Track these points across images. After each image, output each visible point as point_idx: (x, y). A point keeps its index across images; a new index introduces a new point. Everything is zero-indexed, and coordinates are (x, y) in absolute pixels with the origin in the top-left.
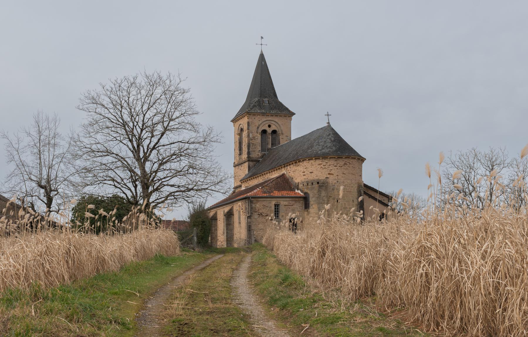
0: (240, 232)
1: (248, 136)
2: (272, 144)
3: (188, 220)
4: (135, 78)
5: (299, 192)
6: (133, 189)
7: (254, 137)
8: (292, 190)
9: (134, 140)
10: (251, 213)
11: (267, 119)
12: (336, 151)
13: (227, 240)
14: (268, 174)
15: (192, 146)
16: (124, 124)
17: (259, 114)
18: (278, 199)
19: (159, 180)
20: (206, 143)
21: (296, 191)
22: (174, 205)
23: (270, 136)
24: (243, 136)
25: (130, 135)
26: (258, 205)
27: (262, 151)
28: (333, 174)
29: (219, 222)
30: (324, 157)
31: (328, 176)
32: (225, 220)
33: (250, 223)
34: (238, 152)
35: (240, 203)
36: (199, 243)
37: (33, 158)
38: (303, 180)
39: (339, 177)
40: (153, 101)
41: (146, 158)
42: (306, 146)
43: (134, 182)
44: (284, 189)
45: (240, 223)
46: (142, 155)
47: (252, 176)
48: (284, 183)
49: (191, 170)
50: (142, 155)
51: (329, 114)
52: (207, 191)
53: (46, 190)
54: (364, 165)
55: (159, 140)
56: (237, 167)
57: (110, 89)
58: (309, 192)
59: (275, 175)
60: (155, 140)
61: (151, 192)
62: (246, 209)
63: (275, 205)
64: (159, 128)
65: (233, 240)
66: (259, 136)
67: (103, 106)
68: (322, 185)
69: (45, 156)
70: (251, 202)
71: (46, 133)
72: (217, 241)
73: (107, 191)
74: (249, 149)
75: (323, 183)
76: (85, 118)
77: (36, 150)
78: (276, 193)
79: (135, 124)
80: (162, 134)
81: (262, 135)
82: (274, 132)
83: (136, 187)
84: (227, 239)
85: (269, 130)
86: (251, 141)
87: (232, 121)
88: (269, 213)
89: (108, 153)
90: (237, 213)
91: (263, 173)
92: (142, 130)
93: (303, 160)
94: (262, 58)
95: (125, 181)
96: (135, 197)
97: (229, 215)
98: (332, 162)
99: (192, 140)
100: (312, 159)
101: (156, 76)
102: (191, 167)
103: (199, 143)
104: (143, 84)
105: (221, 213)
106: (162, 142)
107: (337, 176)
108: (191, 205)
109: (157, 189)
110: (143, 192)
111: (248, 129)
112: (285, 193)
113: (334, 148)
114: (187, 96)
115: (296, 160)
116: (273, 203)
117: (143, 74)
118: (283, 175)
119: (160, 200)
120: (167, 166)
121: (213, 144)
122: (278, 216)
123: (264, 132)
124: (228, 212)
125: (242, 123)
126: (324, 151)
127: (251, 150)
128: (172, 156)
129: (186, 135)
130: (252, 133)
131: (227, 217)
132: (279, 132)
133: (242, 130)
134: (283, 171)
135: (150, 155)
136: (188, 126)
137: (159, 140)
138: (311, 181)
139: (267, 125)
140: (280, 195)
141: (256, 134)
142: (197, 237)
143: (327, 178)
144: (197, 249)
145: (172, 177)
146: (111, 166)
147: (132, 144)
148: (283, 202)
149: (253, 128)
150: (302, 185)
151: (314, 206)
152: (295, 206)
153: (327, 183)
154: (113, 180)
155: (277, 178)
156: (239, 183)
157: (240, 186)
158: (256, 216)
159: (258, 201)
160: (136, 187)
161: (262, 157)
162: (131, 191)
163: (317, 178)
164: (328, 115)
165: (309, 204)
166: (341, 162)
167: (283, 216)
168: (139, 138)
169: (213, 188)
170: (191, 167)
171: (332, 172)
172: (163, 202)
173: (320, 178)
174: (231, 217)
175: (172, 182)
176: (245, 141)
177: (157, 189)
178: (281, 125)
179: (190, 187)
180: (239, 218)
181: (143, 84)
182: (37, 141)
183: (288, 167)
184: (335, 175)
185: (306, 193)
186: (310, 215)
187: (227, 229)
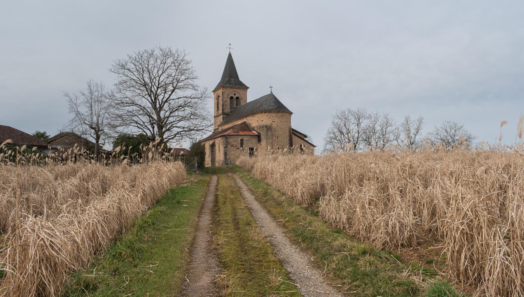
0: (220, 156)
1: (223, 100)
3: (188, 149)
4: (153, 52)
6: (151, 129)
9: (152, 96)
12: (277, 108)
15: (193, 100)
16: (145, 85)
17: (229, 87)
19: (170, 123)
20: (202, 99)
22: (180, 140)
25: (150, 93)
26: (231, 140)
30: (270, 111)
35: (219, 139)
36: (198, 167)
37: (87, 110)
40: (166, 67)
41: (161, 108)
42: (258, 105)
43: (152, 124)
46: (158, 106)
47: (225, 122)
48: (246, 127)
49: (192, 117)
50: (158, 106)
52: (203, 131)
53: (95, 130)
54: (292, 116)
55: (170, 95)
57: (134, 58)
59: (239, 122)
60: (167, 96)
61: (164, 132)
64: (171, 88)
66: (229, 100)
67: (129, 70)
68: (268, 128)
69: (96, 108)
70: (227, 138)
71: (96, 94)
73: (133, 131)
76: (116, 78)
77: (88, 105)
78: (241, 133)
79: (153, 84)
80: (173, 91)
82: (237, 98)
83: (153, 128)
85: (235, 97)
89: (133, 103)
92: (158, 88)
94: (230, 55)
95: (146, 124)
96: (153, 135)
97: (213, 146)
98: (274, 114)
99: (193, 96)
101: (167, 50)
102: (192, 114)
103: (198, 98)
104: (159, 55)
105: (207, 145)
106: (171, 97)
108: (191, 140)
109: (168, 130)
110: (159, 132)
112: (246, 133)
113: (275, 107)
114: (189, 66)
115: (253, 113)
116: (240, 139)
117: (158, 47)
118: (245, 122)
119: (171, 137)
120: (176, 113)
121: (208, 99)
123: (232, 98)
128: (179, 107)
129: (189, 92)
132: (240, 98)
133: (219, 96)
134: (245, 120)
135: (163, 106)
136: (190, 86)
137: (170, 95)
142: (197, 163)
144: (197, 172)
145: (180, 121)
146: (136, 114)
147: (151, 98)
148: (245, 138)
149: (226, 95)
154: (137, 123)
155: (242, 124)
156: (217, 127)
157: (218, 129)
158: (229, 146)
160: (153, 128)
161: (231, 112)
162: (150, 131)
166: (280, 115)
168: (156, 94)
169: (207, 129)
170: (192, 114)
172: (172, 138)
175: (178, 125)
176: (221, 103)
177: (168, 130)
179: (192, 128)
180: (219, 148)
181: (159, 55)
182: (89, 98)
185: (259, 133)
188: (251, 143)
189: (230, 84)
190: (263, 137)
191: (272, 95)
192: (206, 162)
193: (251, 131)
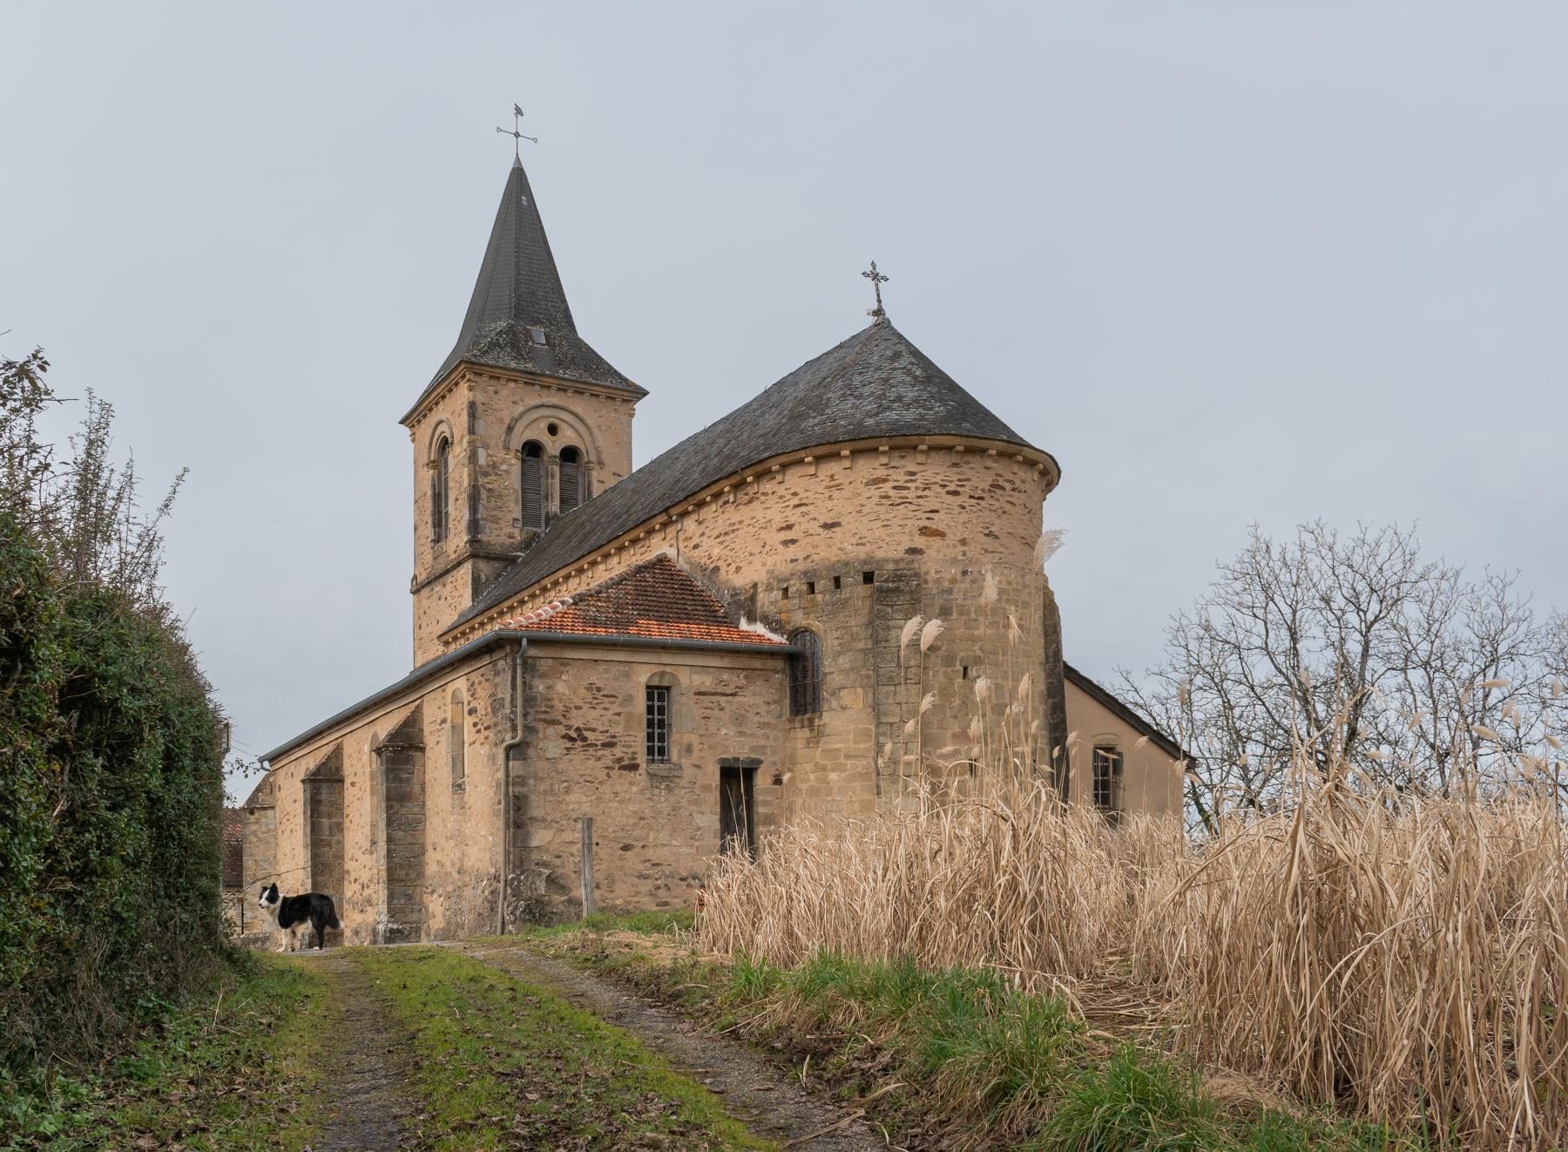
1: (473, 458)
2: (562, 501)
5: (760, 628)
7: (494, 466)
8: (728, 621)
10: (529, 729)
11: (545, 400)
13: (391, 879)
17: (513, 376)
21: (744, 625)
23: (557, 469)
24: (451, 461)
26: (565, 686)
27: (524, 524)
28: (942, 535)
29: (350, 793)
31: (920, 542)
32: (380, 778)
33: (521, 781)
34: (429, 532)
35: (459, 683)
38: (784, 569)
39: (972, 550)
44: (688, 618)
45: (458, 787)
48: (672, 594)
51: (881, 271)
54: (1056, 509)
56: (425, 592)
58: (816, 625)
62: (496, 705)
63: (650, 690)
65: (421, 875)
66: (513, 465)
68: (889, 588)
70: (529, 667)
72: (341, 881)
74: (474, 509)
75: (898, 577)
78: (655, 631)
81: (523, 461)
82: (570, 454)
84: (389, 870)
85: (553, 446)
86: (482, 480)
87: (402, 422)
88: (618, 730)
90: (445, 737)
91: (547, 582)
93: (785, 467)
94: (518, 181)
97: (402, 751)
98: (936, 470)
100: (836, 456)
107: (963, 542)
111: (472, 431)
112: (695, 632)
116: (643, 676)
122: (662, 751)
123: (532, 450)
124: (393, 737)
125: (443, 416)
126: (891, 415)
127: (481, 513)
130: (486, 447)
131: (389, 761)
134: (660, 546)
138: (832, 567)
139: (544, 425)
140: (678, 639)
141: (501, 454)
143: (913, 551)
149: (491, 430)
150: (777, 594)
151: (846, 697)
152: (746, 699)
153: (917, 575)
155: (622, 579)
158: (551, 744)
159: (564, 662)
161: (526, 545)
163: (861, 553)
164: (875, 277)
165: (816, 689)
167: (689, 749)
171: (938, 522)
173: (880, 554)
174: (409, 760)
176: (459, 477)
178: (596, 431)
180: (457, 762)
183: (690, 524)
184: (952, 538)
185: (794, 634)
186: (827, 743)
187: (389, 824)
188: (739, 719)
189: (519, 356)
190: (836, 669)
191: (882, 340)
192: (350, 890)
193: (728, 621)
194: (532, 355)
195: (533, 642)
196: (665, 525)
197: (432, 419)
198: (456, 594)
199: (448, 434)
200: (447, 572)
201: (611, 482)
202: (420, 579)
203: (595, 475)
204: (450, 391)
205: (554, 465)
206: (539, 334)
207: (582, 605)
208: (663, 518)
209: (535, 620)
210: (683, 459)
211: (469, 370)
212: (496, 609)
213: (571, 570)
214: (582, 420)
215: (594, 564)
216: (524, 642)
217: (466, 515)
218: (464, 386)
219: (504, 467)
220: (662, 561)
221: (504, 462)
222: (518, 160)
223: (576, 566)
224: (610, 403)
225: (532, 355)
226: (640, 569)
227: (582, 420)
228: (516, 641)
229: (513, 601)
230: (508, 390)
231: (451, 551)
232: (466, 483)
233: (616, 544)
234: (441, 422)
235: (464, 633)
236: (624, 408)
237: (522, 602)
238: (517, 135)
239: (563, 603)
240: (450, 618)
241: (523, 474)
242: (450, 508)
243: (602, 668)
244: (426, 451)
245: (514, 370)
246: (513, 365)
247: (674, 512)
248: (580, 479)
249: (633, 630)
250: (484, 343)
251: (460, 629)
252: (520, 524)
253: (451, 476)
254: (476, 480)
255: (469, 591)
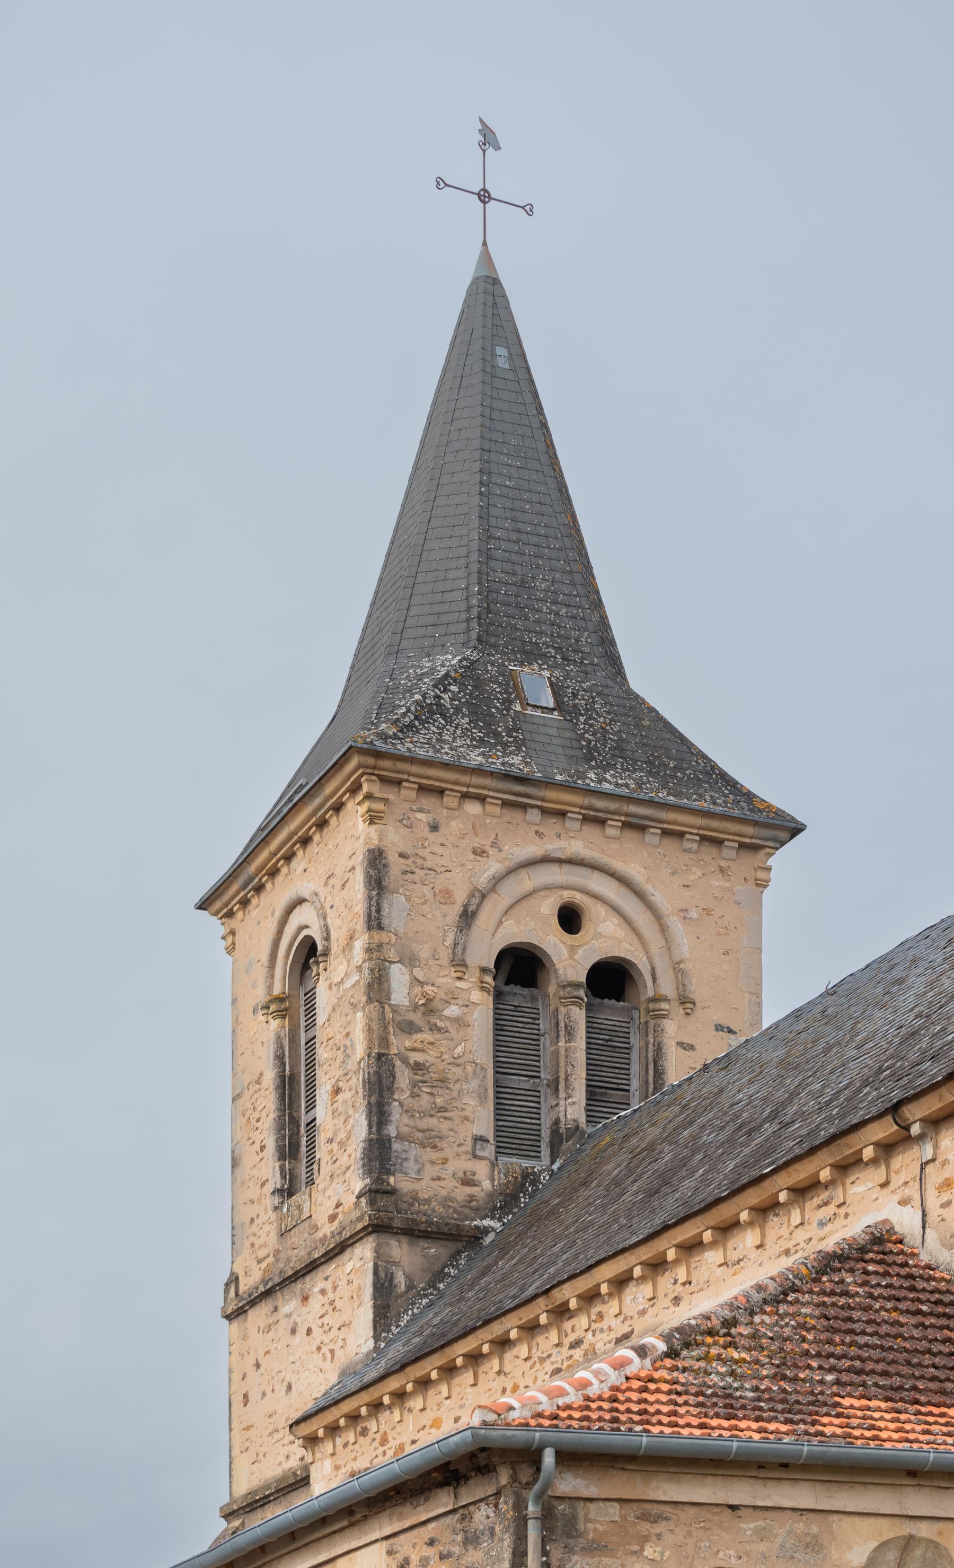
1: (377, 987)
2: (592, 1094)
11: (554, 846)
14: (636, 1295)
17: (471, 786)
18: (919, 1501)
23: (579, 1015)
24: (324, 998)
27: (500, 1150)
34: (268, 1169)
56: (258, 1316)
66: (474, 1006)
74: (378, 1113)
81: (498, 996)
85: (571, 960)
87: (203, 905)
91: (569, 1294)
94: (488, 309)
111: (374, 921)
123: (520, 967)
125: (303, 888)
127: (398, 1122)
130: (410, 960)
134: (869, 1204)
139: (549, 907)
141: (446, 979)
149: (422, 918)
155: (784, 1293)
159: (651, 1512)
161: (506, 1201)
178: (675, 924)
189: (490, 737)
194: (518, 734)
195: (570, 1458)
196: (887, 1149)
197: (277, 896)
198: (332, 1320)
199: (316, 933)
200: (312, 1267)
201: (713, 1047)
202: (245, 1285)
203: (672, 1029)
204: (322, 824)
205: (569, 1005)
206: (537, 685)
207: (689, 1358)
208: (884, 1130)
209: (574, 1398)
210: (917, 982)
211: (371, 771)
212: (438, 1360)
213: (632, 1262)
214: (640, 895)
215: (692, 1247)
216: (549, 1458)
217: (360, 1129)
218: (355, 811)
219: (453, 1010)
220: (881, 1244)
221: (452, 997)
222: (486, 257)
223: (645, 1253)
224: (709, 851)
225: (518, 734)
226: (829, 1263)
227: (640, 895)
228: (529, 1456)
229: (481, 1340)
230: (464, 821)
231: (321, 1217)
232: (360, 1050)
233: (754, 1197)
234: (300, 901)
235: (354, 1418)
236: (743, 865)
237: (503, 1343)
238: (484, 196)
239: (642, 1351)
240: (316, 1380)
241: (499, 1028)
242: (321, 1112)
243: (749, 1525)
244: (260, 972)
245: (478, 771)
246: (476, 758)
247: (916, 1113)
248: (636, 1040)
249: (831, 1426)
250: (404, 706)
251: (347, 1407)
252: (489, 1151)
253: (321, 1034)
254: (384, 1041)
255: (365, 1315)
